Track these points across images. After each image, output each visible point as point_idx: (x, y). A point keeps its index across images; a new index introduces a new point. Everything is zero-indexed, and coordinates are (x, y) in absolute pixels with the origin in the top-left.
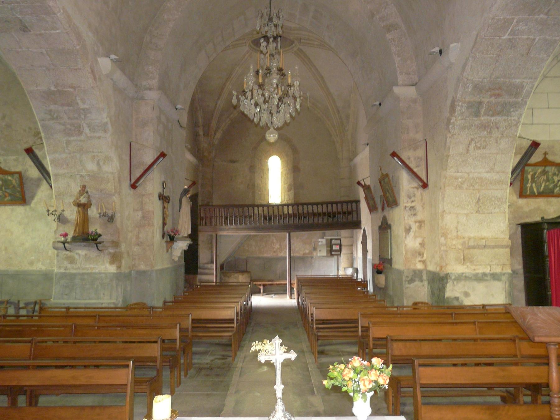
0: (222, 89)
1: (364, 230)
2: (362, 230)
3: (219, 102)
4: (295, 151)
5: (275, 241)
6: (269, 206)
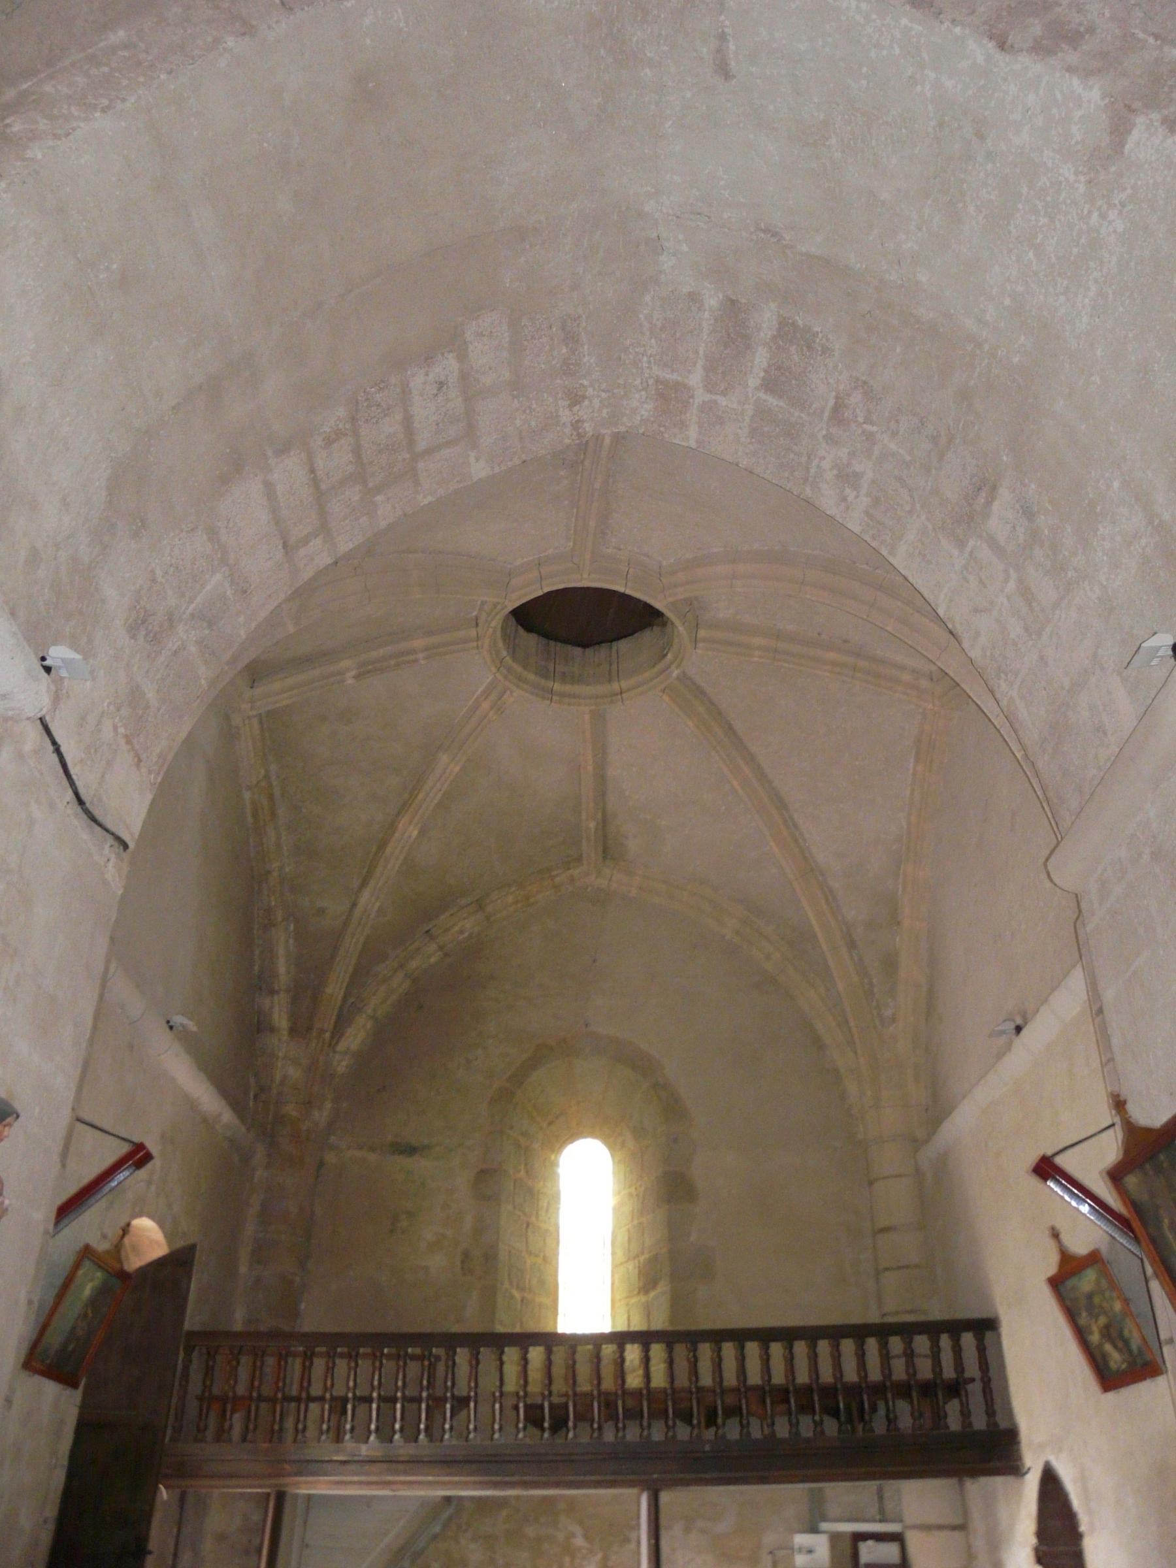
0: (383, 845)
1: (1049, 1479)
2: (1032, 1483)
3: (365, 897)
4: (672, 1108)
5: (579, 1541)
6: (551, 1340)
